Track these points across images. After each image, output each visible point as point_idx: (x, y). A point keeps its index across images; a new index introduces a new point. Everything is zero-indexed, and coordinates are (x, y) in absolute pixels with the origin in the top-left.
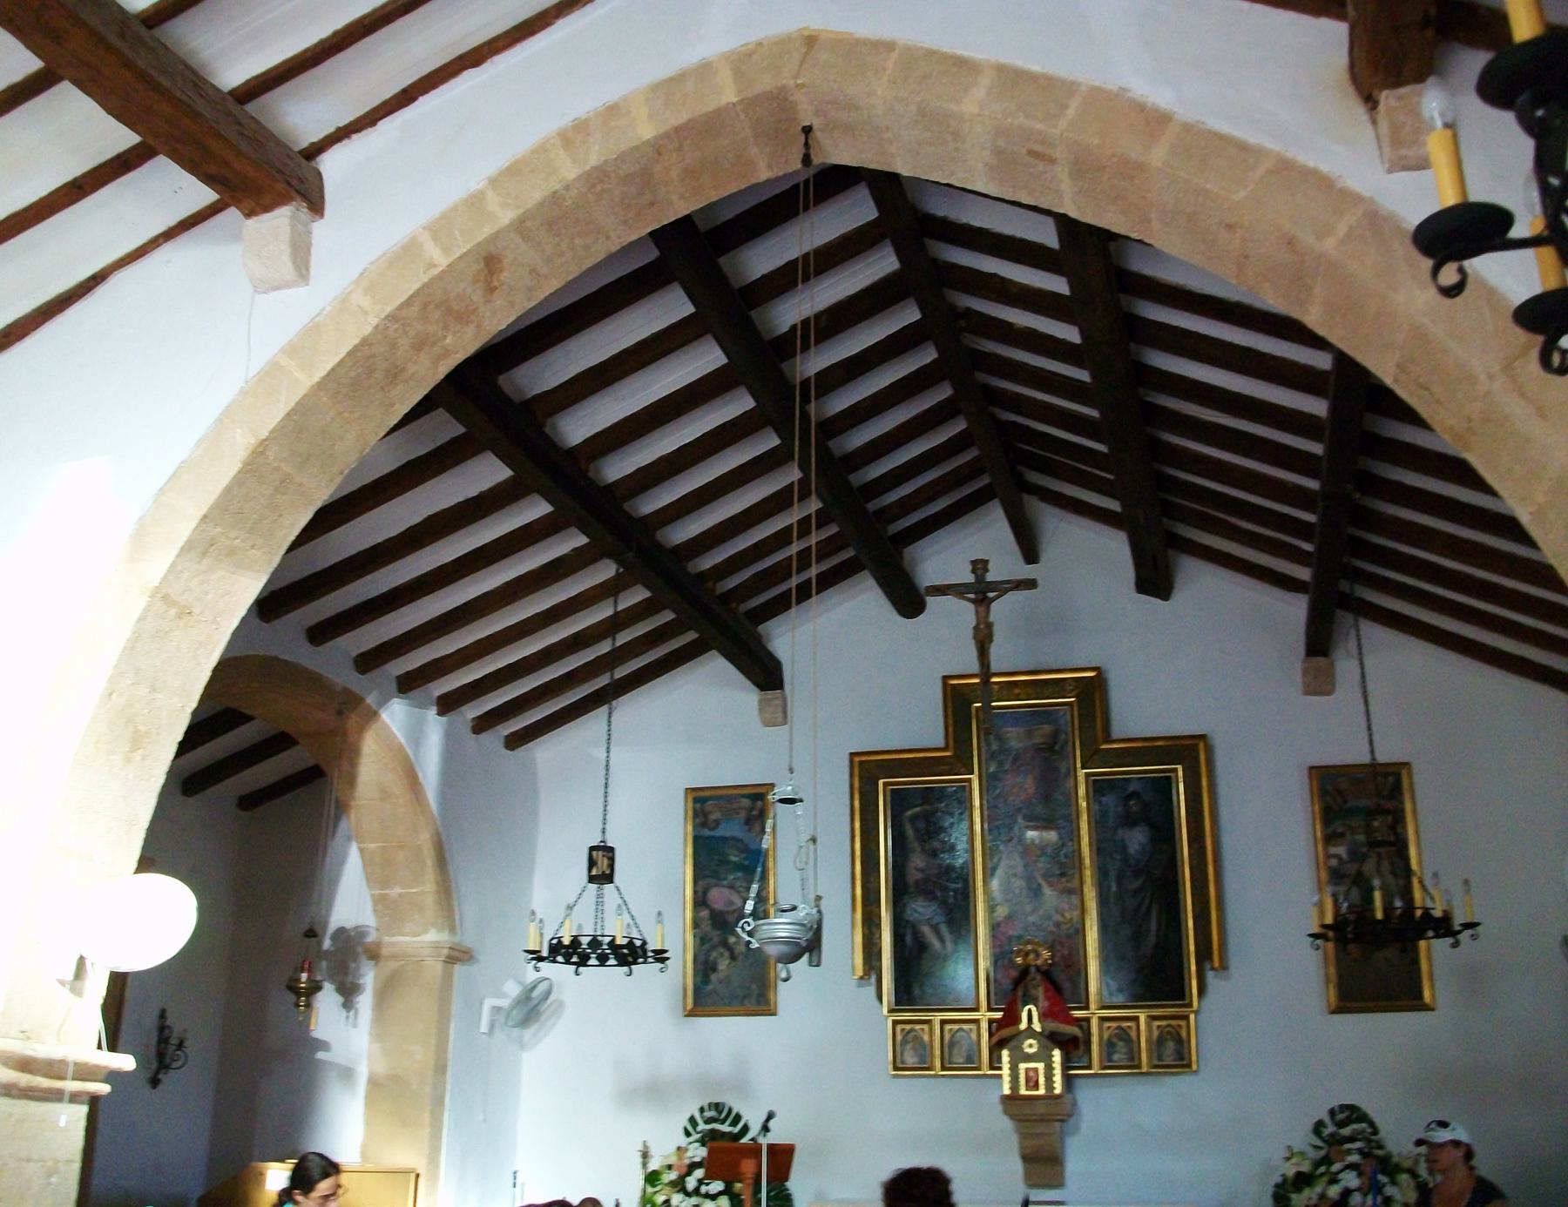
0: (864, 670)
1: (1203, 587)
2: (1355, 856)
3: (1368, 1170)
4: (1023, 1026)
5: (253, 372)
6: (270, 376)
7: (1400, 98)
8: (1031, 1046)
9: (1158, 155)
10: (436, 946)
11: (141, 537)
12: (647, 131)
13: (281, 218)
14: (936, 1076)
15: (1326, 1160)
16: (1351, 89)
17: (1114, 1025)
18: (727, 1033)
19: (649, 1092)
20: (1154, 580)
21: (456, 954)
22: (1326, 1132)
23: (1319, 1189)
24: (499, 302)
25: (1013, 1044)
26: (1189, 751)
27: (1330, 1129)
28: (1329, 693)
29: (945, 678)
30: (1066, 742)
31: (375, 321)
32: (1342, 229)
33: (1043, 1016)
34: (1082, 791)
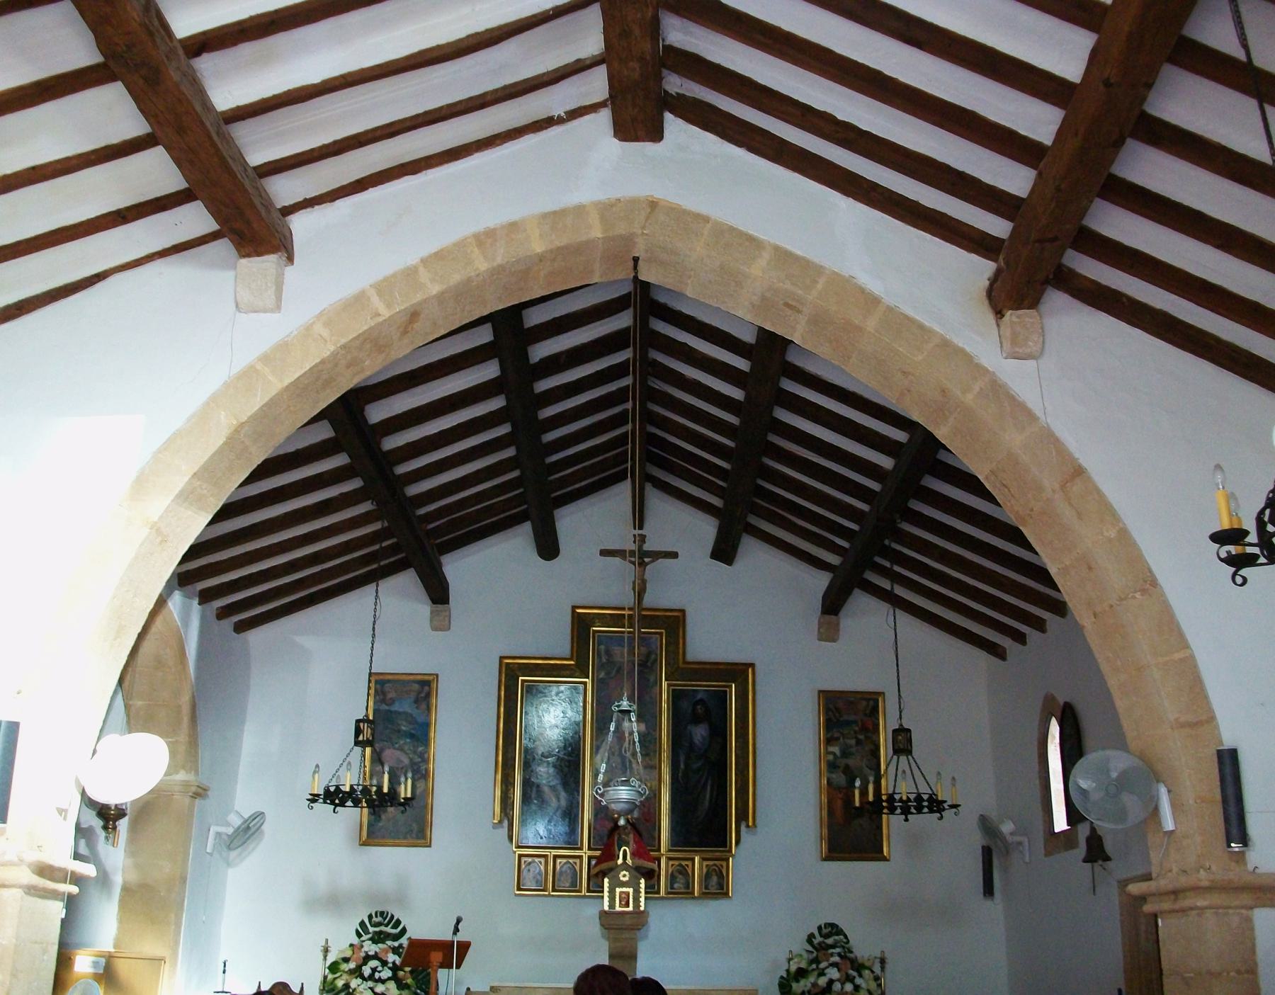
0: (509, 590)
1: (756, 557)
2: (845, 754)
3: (843, 967)
4: (620, 861)
5: (235, 371)
6: (248, 376)
7: (1018, 317)
8: (624, 876)
9: (871, 324)
10: (186, 784)
11: (142, 484)
12: (538, 247)
13: (269, 262)
14: (549, 895)
15: (816, 961)
16: (986, 302)
17: (677, 863)
18: (393, 861)
19: (329, 902)
20: (724, 552)
21: (200, 791)
22: (816, 942)
23: (812, 979)
24: (406, 341)
25: (612, 873)
26: (739, 673)
27: (818, 939)
28: (834, 640)
29: (574, 608)
30: (656, 660)
31: (332, 348)
32: (976, 388)
33: (633, 854)
34: (664, 696)
